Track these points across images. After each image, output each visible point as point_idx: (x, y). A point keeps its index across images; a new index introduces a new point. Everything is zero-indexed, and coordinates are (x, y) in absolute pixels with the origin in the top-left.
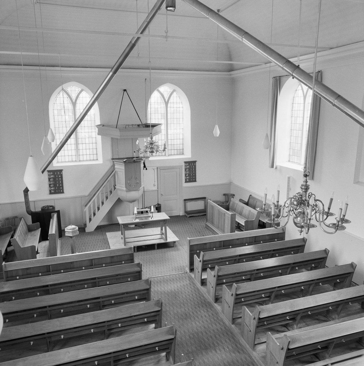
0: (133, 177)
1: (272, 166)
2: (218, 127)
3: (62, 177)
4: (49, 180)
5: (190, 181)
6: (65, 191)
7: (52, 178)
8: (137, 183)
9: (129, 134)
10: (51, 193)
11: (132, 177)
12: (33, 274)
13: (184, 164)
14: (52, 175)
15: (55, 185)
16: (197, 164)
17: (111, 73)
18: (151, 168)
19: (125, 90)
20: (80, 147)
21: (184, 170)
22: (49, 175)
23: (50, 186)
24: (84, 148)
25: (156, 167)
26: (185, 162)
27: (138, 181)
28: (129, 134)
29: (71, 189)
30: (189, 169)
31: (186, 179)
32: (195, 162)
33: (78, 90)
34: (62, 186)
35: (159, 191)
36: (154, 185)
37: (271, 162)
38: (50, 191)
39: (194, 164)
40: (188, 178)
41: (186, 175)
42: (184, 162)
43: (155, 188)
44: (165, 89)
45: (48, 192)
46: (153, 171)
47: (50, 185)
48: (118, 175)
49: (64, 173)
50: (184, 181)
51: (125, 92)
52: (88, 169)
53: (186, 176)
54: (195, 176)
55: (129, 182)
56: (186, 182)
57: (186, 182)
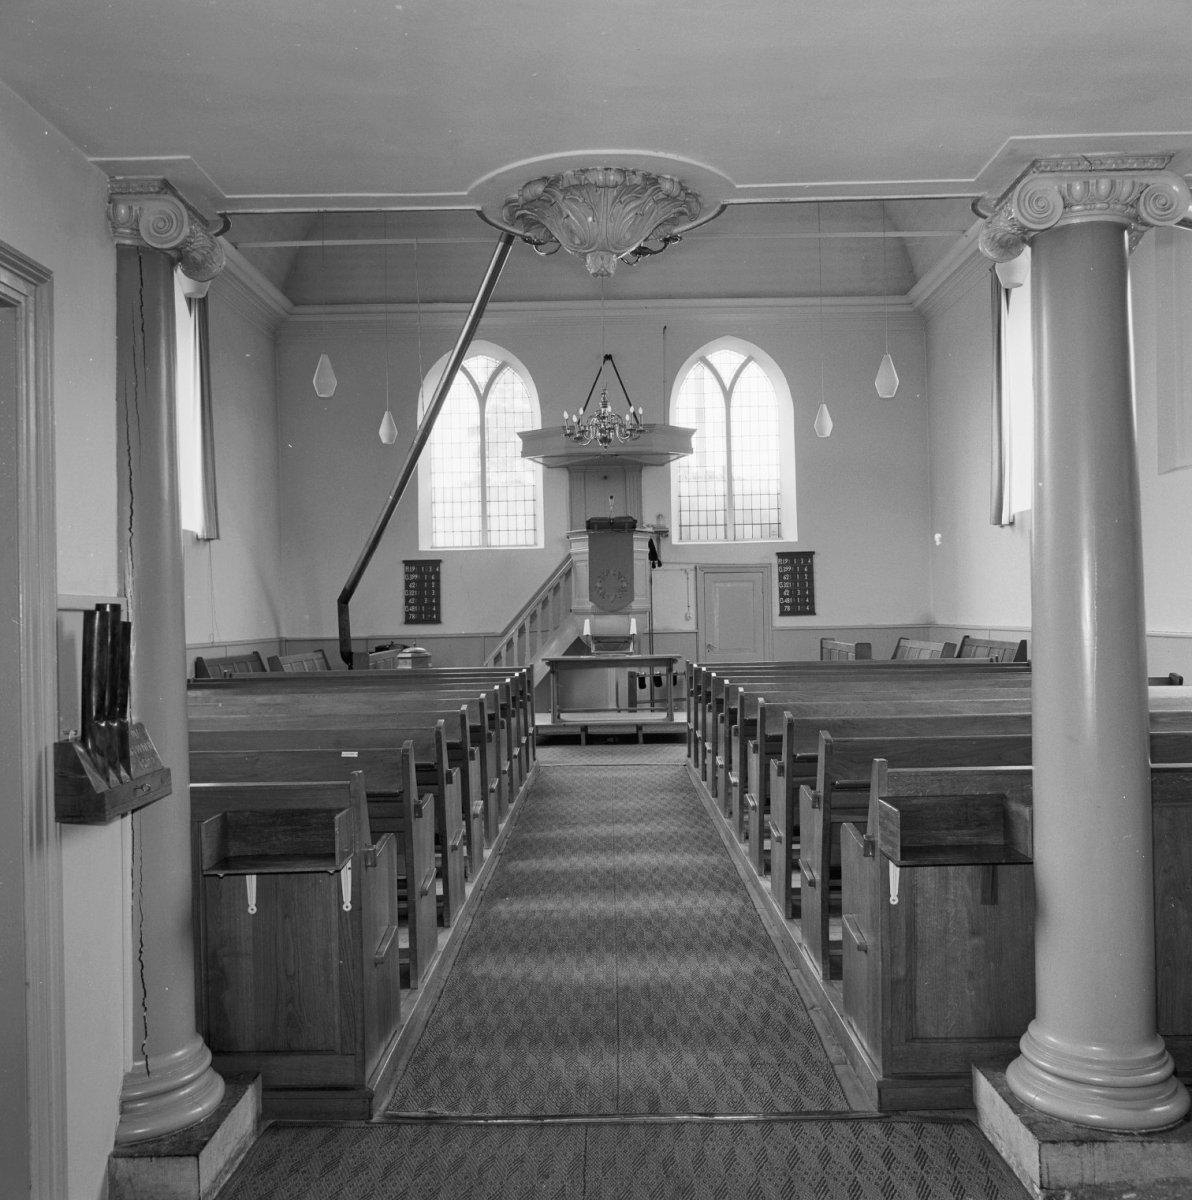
0: (612, 572)
1: (998, 520)
2: (826, 408)
3: (438, 581)
4: (407, 587)
5: (794, 613)
6: (443, 618)
7: (414, 580)
8: (623, 590)
9: (608, 470)
10: (408, 621)
11: (608, 572)
12: (812, 1120)
13: (775, 561)
14: (414, 573)
15: (419, 599)
16: (816, 560)
17: (501, 244)
18: (678, 567)
19: (608, 357)
20: (492, 509)
21: (775, 576)
22: (406, 573)
23: (407, 603)
24: (503, 511)
25: (692, 567)
26: (780, 555)
27: (625, 585)
28: (608, 470)
29: (458, 615)
30: (792, 574)
31: (782, 606)
32: (810, 555)
33: (493, 364)
34: (438, 604)
35: (701, 637)
36: (687, 618)
37: (994, 505)
38: (407, 614)
39: (806, 562)
40: (788, 601)
41: (781, 591)
42: (404, 562)
43: (691, 626)
44: (726, 357)
45: (401, 617)
46: (685, 576)
47: (407, 598)
48: (576, 574)
49: (444, 569)
50: (776, 610)
51: (608, 362)
52: (508, 561)
53: (781, 595)
54: (812, 596)
55: (599, 585)
56: (783, 613)
57: (783, 613)
